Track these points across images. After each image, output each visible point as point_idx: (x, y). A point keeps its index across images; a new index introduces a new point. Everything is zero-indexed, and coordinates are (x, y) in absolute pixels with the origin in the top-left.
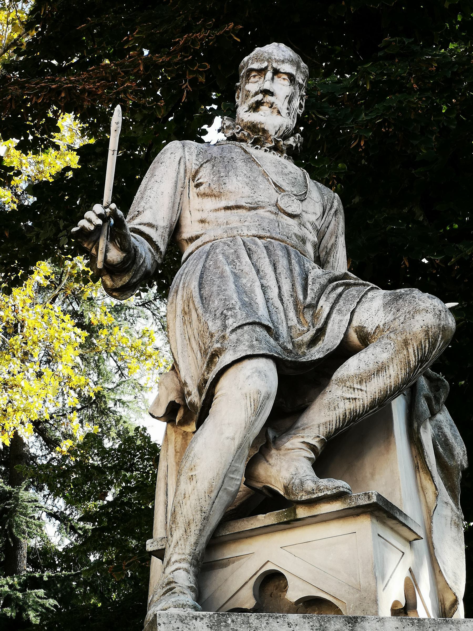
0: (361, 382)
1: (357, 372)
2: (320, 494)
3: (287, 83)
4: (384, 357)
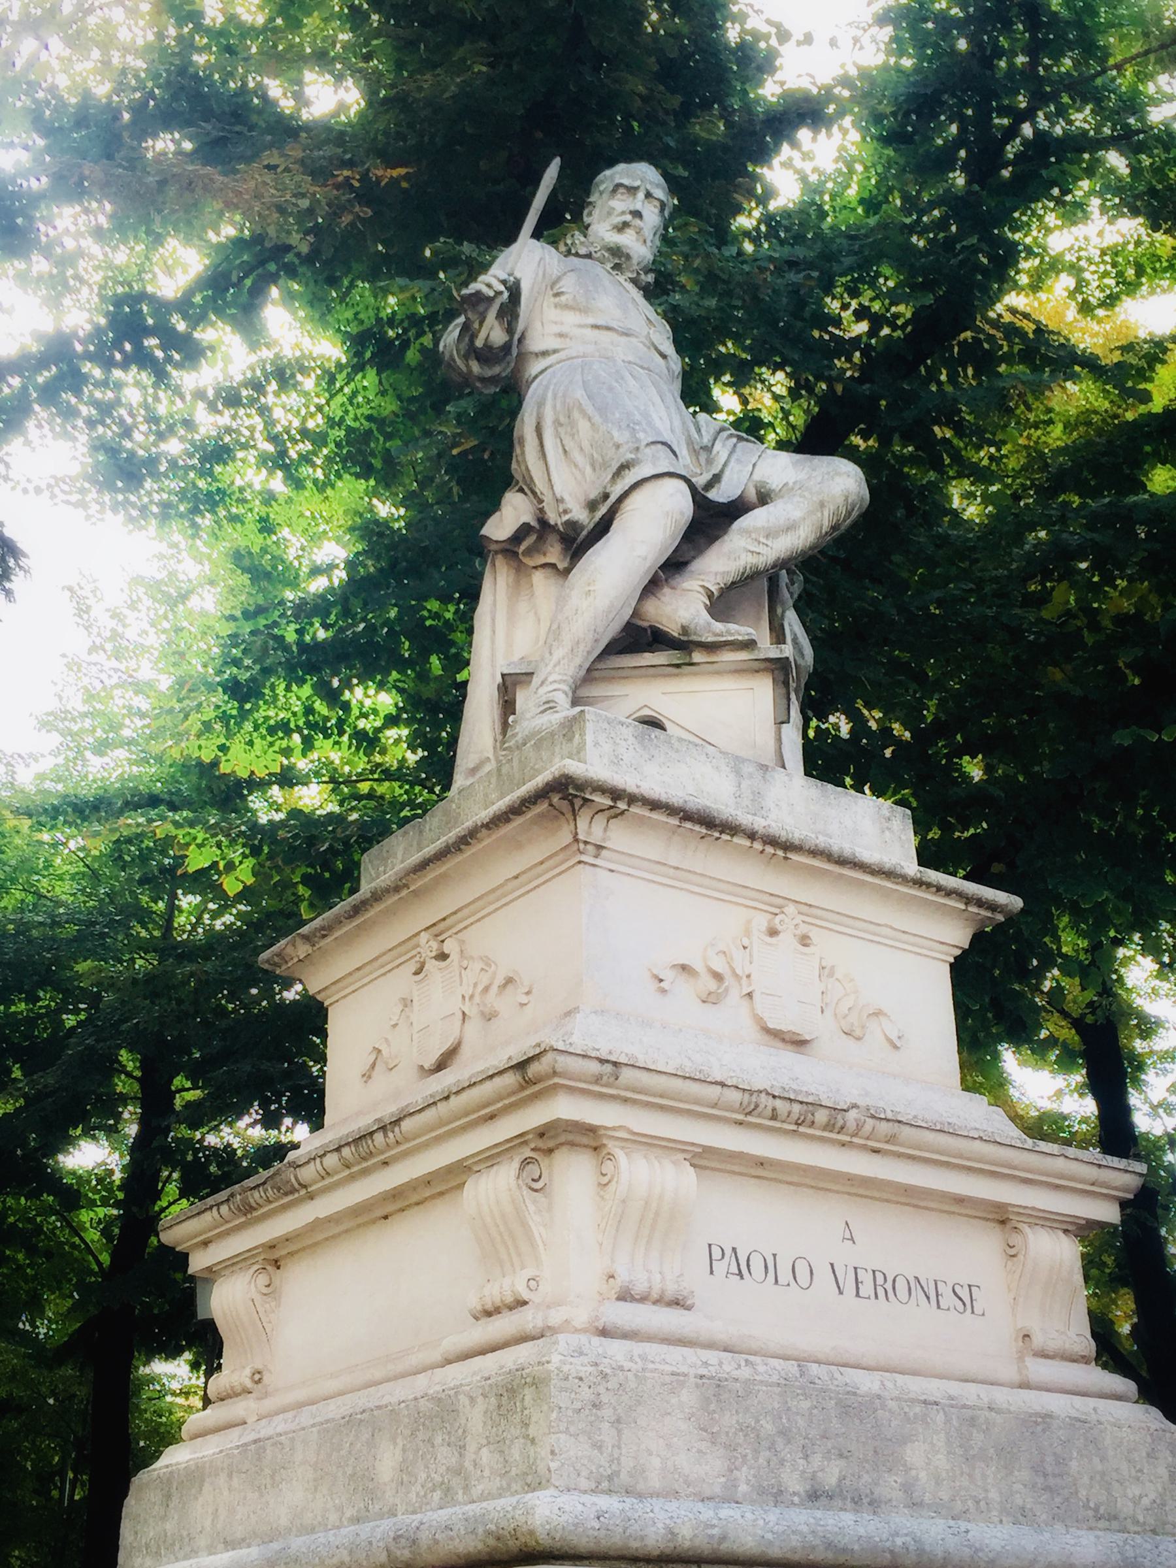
0: (767, 537)
1: (766, 525)
2: (730, 638)
3: (657, 211)
4: (797, 514)
